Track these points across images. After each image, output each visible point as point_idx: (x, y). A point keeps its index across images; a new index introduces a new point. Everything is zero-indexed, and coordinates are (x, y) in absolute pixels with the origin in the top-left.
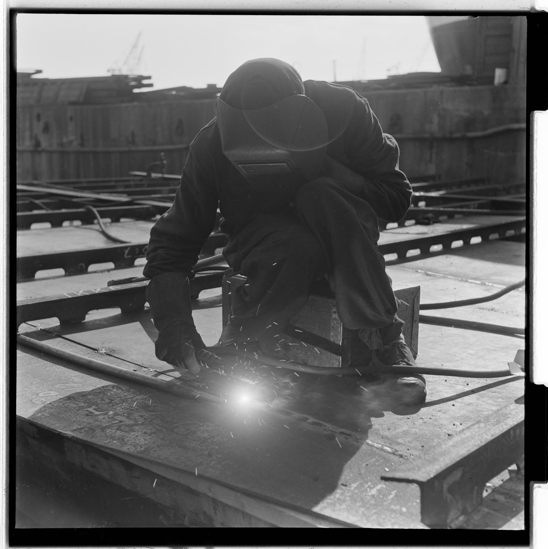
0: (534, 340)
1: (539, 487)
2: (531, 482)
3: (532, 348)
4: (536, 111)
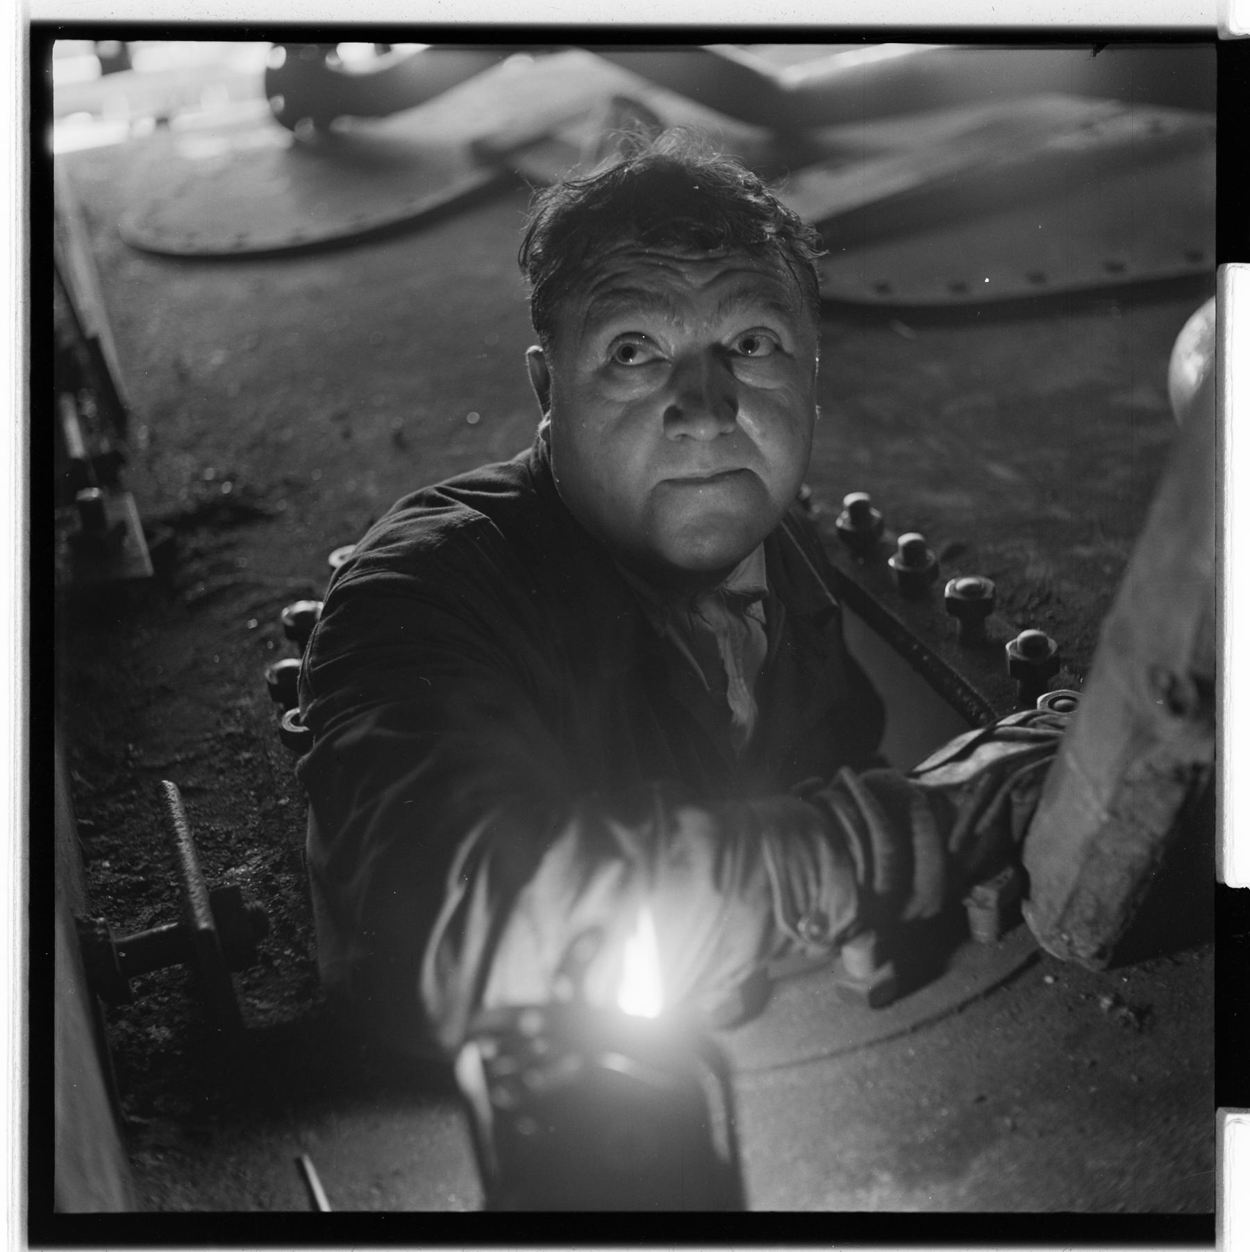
0: (1227, 787)
1: (1238, 1121)
3: (1222, 805)
4: (1230, 265)
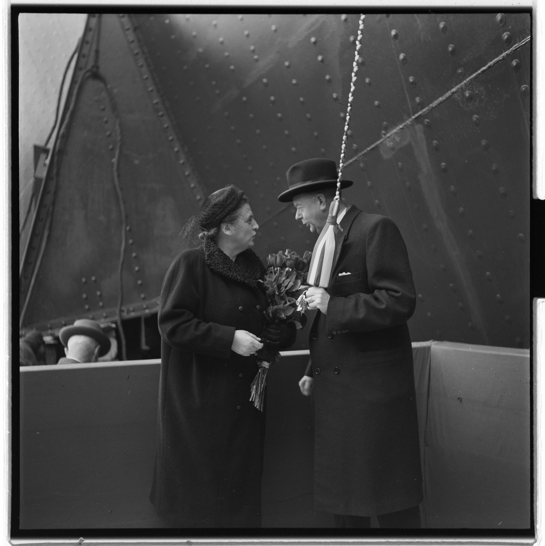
2: (535, 299)
